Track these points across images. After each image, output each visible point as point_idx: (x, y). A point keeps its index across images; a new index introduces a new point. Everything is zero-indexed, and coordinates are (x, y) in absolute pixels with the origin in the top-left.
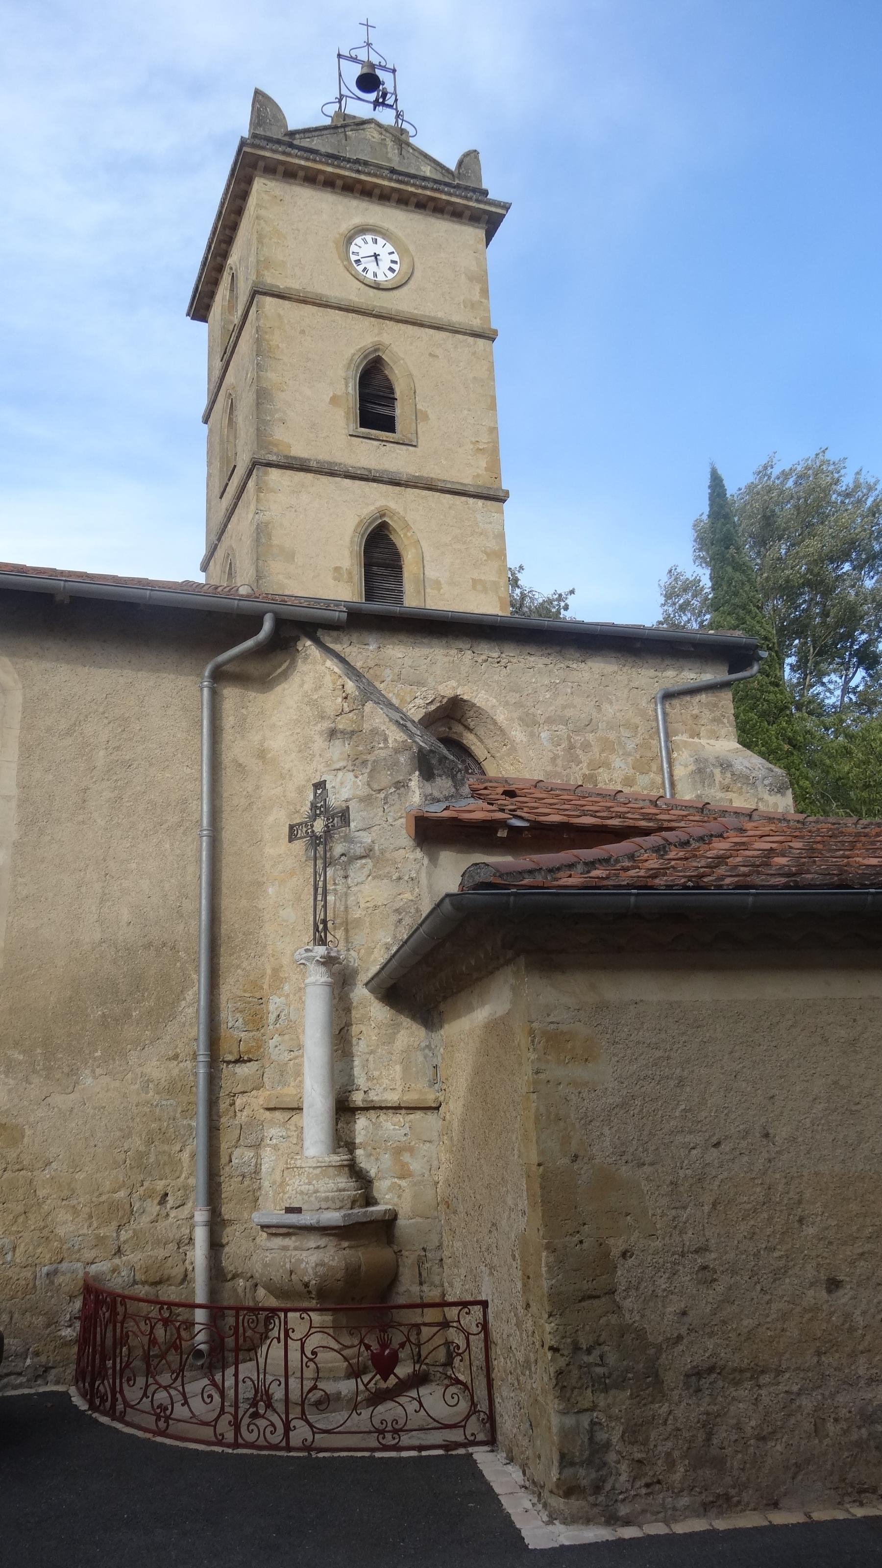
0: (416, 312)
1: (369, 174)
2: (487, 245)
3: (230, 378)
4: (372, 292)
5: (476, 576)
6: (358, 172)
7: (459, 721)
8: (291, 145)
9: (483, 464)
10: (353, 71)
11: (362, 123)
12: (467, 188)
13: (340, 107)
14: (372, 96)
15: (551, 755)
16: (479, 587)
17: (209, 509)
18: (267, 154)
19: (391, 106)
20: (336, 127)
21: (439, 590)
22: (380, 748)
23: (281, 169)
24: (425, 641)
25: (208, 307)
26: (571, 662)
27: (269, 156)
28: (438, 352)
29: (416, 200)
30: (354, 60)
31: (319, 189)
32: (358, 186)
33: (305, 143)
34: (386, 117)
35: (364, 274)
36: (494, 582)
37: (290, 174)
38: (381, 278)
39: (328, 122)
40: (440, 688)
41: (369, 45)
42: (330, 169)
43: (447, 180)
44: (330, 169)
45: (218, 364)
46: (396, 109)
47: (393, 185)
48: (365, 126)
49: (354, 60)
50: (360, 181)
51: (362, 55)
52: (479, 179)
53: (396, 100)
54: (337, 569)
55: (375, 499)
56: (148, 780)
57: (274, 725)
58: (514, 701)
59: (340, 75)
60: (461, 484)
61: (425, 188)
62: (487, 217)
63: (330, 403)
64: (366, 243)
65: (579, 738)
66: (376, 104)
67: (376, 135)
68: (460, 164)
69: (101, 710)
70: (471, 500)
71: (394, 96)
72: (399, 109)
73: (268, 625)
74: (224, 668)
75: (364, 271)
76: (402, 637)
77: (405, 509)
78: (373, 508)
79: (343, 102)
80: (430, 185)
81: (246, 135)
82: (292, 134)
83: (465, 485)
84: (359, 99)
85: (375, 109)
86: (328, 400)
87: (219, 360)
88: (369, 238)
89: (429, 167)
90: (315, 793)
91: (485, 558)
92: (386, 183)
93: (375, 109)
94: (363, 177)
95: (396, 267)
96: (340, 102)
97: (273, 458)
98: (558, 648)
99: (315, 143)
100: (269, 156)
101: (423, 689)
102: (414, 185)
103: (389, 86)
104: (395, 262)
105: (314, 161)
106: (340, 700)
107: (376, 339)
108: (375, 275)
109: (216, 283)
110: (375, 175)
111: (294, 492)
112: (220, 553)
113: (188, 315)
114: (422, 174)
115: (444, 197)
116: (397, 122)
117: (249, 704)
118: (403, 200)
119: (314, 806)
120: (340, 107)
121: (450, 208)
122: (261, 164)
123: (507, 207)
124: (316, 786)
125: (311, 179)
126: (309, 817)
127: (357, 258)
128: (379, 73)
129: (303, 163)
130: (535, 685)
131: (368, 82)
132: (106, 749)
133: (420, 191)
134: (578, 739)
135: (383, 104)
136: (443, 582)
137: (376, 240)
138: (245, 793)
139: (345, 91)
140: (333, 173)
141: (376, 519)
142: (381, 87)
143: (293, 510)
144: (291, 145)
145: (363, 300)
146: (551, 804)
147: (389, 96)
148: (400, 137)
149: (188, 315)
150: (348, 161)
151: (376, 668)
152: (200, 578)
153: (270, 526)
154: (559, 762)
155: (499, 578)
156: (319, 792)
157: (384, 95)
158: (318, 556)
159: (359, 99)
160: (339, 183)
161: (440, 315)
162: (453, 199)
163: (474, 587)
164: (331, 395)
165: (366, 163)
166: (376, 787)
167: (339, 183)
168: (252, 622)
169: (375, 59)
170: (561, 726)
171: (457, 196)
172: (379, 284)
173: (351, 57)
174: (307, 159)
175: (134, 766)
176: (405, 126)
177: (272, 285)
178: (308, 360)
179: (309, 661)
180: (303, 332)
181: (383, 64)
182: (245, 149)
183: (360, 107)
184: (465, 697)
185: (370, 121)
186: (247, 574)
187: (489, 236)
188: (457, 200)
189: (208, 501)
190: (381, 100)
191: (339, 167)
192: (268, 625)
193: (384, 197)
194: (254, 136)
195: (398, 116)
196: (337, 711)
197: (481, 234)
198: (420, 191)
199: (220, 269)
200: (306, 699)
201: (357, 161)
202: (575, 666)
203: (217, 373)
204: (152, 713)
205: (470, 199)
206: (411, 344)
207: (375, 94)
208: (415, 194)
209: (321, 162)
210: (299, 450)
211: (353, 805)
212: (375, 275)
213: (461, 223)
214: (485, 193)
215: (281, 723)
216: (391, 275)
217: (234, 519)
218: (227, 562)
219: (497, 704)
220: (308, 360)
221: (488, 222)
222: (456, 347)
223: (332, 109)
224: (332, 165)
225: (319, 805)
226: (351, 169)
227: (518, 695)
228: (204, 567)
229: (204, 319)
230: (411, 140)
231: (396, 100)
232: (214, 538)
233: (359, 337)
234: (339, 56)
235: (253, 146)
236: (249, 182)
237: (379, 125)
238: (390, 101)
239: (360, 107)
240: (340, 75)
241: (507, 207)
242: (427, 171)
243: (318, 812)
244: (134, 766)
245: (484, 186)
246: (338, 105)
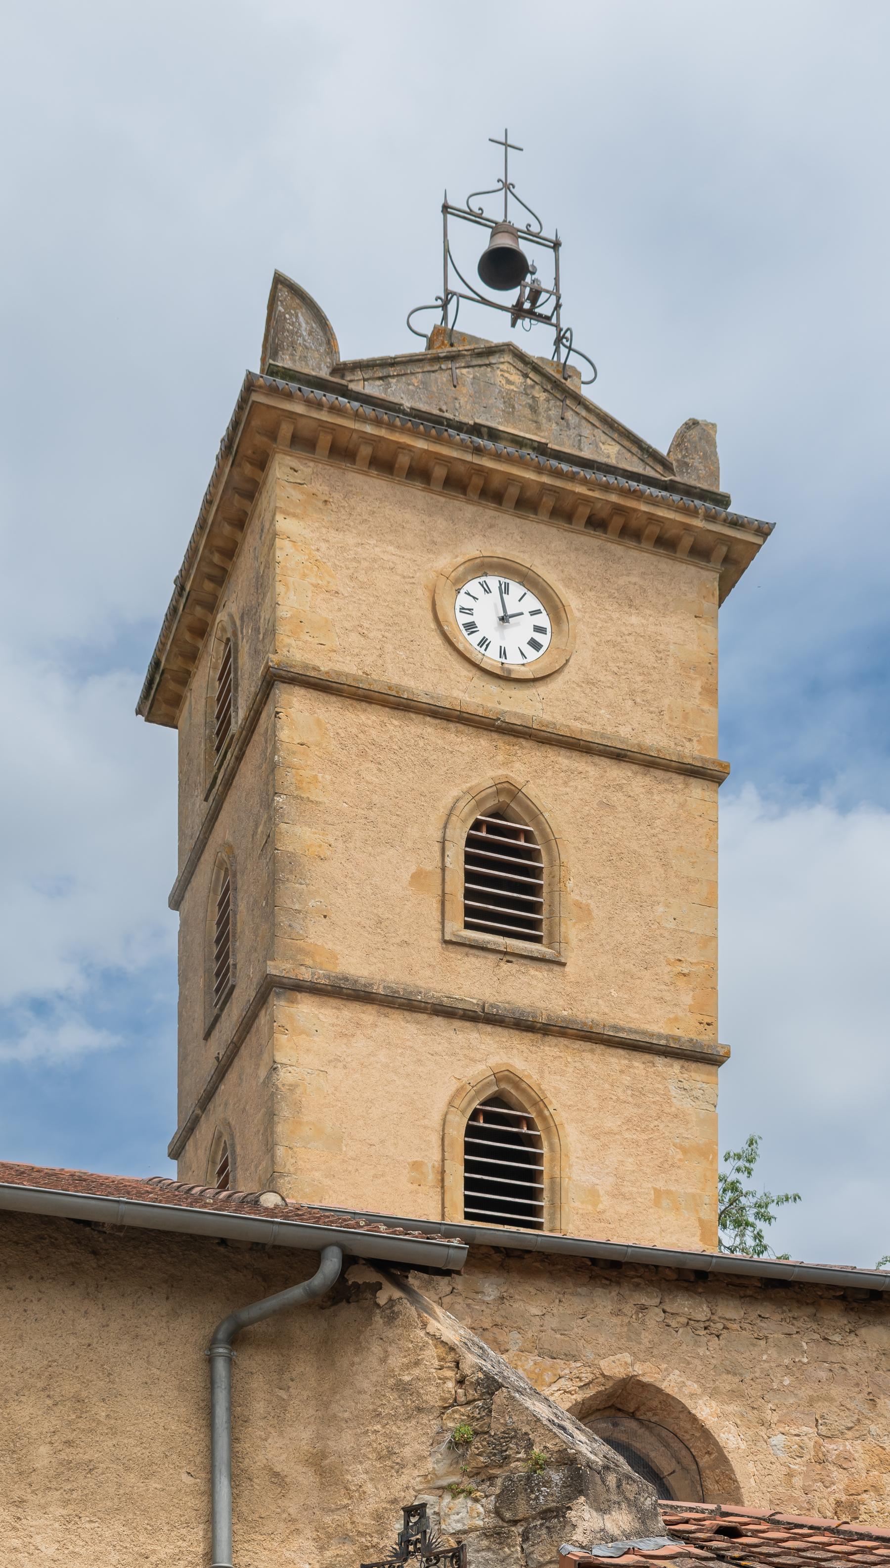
0: (577, 725)
1: (497, 456)
2: (721, 600)
3: (222, 832)
4: (494, 688)
5: (660, 1185)
6: (478, 451)
7: (633, 1415)
8: (344, 392)
9: (687, 999)
10: (472, 244)
11: (488, 352)
12: (689, 491)
13: (445, 318)
14: (510, 297)
15: (784, 1470)
16: (665, 1202)
17: (183, 1057)
18: (299, 408)
19: (546, 319)
20: (437, 359)
21: (595, 1205)
22: (518, 1460)
23: (325, 440)
24: (582, 1290)
25: (177, 701)
26: (830, 1332)
27: (302, 416)
28: (617, 798)
29: (588, 511)
30: (475, 217)
31: (400, 483)
32: (478, 481)
33: (373, 389)
34: (536, 341)
35: (482, 650)
36: (693, 1196)
37: (342, 452)
38: (513, 659)
39: (419, 346)
40: (603, 1364)
41: (507, 187)
42: (421, 444)
43: (649, 472)
44: (421, 444)
45: (200, 807)
46: (557, 326)
47: (546, 479)
48: (493, 360)
49: (475, 217)
50: (480, 470)
51: (493, 209)
52: (714, 475)
53: (558, 306)
54: (416, 1166)
55: (492, 1055)
56: (121, 1492)
57: (335, 1416)
58: (728, 1387)
59: (447, 251)
60: (644, 1033)
61: (606, 488)
62: (724, 549)
63: (411, 884)
64: (488, 591)
65: (833, 1446)
66: (518, 312)
67: (517, 378)
68: (680, 441)
69: (40, 1385)
70: (660, 1061)
71: (553, 299)
72: (564, 326)
73: (331, 1264)
74: (250, 1328)
75: (481, 644)
76: (542, 1284)
77: (541, 1072)
78: (481, 1067)
79: (452, 307)
80: (368, 410)
81: (256, 369)
82: (340, 369)
83: (652, 1035)
84: (484, 301)
85: (513, 325)
86: (406, 877)
87: (202, 797)
88: (493, 582)
89: (617, 448)
90: (407, 1522)
91: (680, 1156)
92: (530, 476)
93: (513, 325)
94: (488, 463)
95: (544, 640)
96: (444, 307)
97: (305, 975)
98: (811, 1310)
99: (400, 393)
100: (302, 416)
101: (573, 1365)
102: (584, 482)
103: (544, 276)
104: (539, 629)
105: (391, 427)
106: (450, 1385)
107: (501, 772)
108: (503, 653)
109: (192, 656)
110: (509, 459)
111: (343, 1035)
112: (205, 1132)
113: (139, 712)
114: (602, 459)
115: (644, 508)
116: (557, 350)
117: (291, 1384)
118: (564, 513)
119: (404, 1539)
120: (445, 318)
121: (655, 530)
122: (286, 430)
123: (764, 531)
124: (410, 1511)
125: (383, 463)
126: (396, 1555)
127: (468, 619)
128: (525, 248)
129: (369, 429)
130: (766, 1365)
131: (502, 266)
132: (51, 1443)
133: (596, 494)
134: (832, 1447)
135: (531, 314)
136: (602, 1193)
137: (507, 586)
138: (285, 1516)
139: (455, 285)
140: (426, 451)
141: (489, 1085)
142: (529, 278)
143: (340, 1065)
144: (344, 392)
145: (478, 700)
146: (799, 1550)
147: (543, 296)
148: (556, 383)
149: (139, 712)
150: (460, 427)
151: (495, 1330)
152: (170, 1171)
153: (298, 1091)
154: (798, 1481)
155: (703, 1189)
156: (413, 1520)
157: (535, 295)
158: (382, 1142)
159: (484, 301)
160: (439, 472)
161: (624, 731)
162: (661, 512)
163: (657, 1203)
164: (413, 869)
165: (494, 435)
166: (508, 1515)
167: (439, 472)
168: (307, 1258)
169: (519, 219)
170: (805, 1429)
171: (670, 506)
172: (509, 671)
173: (471, 212)
174: (378, 422)
175: (100, 1471)
176: (574, 361)
177: (306, 666)
178: (371, 806)
179: (398, 1322)
180: (363, 754)
181: (535, 228)
182: (255, 397)
183: (485, 320)
184: (645, 1379)
185: (509, 349)
186: (256, 1167)
187: (725, 587)
188: (667, 517)
189: (182, 1043)
190: (527, 305)
191: (438, 440)
192: (331, 1264)
193: (526, 503)
194: (272, 371)
195: (558, 341)
196: (444, 1400)
197: (711, 578)
198: (596, 494)
199: (201, 631)
200: (391, 1381)
201: (476, 430)
202: (837, 1338)
203: (196, 823)
204: (127, 1392)
205: (694, 513)
206: (565, 783)
207: (516, 291)
208: (586, 500)
209: (403, 430)
210: (356, 965)
211: (470, 1539)
212: (503, 653)
213: (674, 559)
214: (723, 501)
215: (346, 1415)
216: (532, 654)
217: (232, 1076)
218: (218, 1145)
219: (699, 1391)
220: (371, 806)
221: (726, 560)
222: (650, 792)
223: (428, 322)
224: (426, 436)
225: (414, 1539)
226: (462, 446)
227: (737, 1379)
228: (176, 1152)
229: (170, 722)
230: (586, 392)
231: (558, 306)
232: (191, 1103)
233: (475, 768)
234: (446, 208)
235: (273, 391)
236: (262, 463)
237: (520, 356)
238: (545, 309)
239: (485, 320)
240: (447, 251)
241: (764, 531)
242: (610, 452)
243: (411, 1548)
244: (100, 1471)
245: (723, 489)
246: (440, 312)
